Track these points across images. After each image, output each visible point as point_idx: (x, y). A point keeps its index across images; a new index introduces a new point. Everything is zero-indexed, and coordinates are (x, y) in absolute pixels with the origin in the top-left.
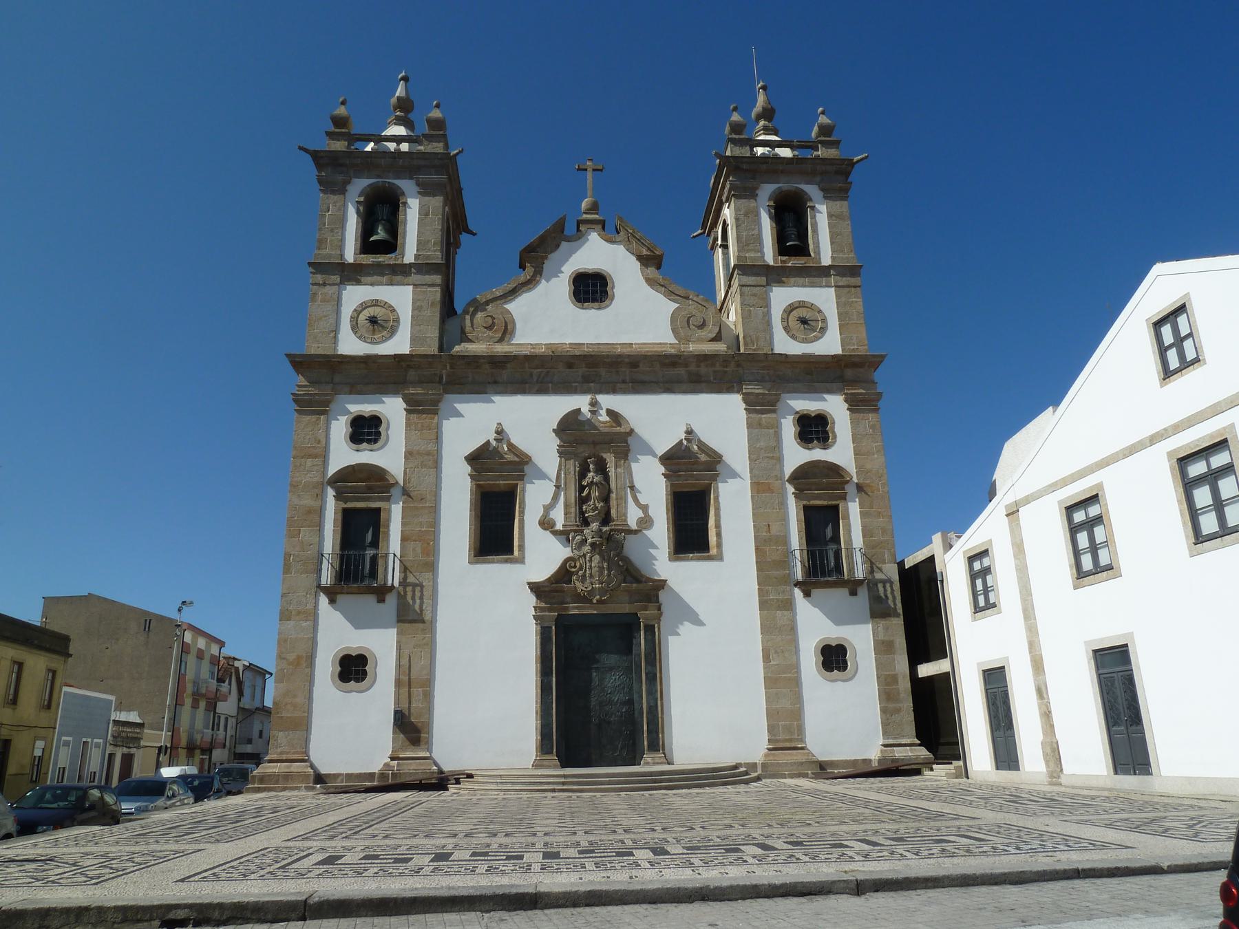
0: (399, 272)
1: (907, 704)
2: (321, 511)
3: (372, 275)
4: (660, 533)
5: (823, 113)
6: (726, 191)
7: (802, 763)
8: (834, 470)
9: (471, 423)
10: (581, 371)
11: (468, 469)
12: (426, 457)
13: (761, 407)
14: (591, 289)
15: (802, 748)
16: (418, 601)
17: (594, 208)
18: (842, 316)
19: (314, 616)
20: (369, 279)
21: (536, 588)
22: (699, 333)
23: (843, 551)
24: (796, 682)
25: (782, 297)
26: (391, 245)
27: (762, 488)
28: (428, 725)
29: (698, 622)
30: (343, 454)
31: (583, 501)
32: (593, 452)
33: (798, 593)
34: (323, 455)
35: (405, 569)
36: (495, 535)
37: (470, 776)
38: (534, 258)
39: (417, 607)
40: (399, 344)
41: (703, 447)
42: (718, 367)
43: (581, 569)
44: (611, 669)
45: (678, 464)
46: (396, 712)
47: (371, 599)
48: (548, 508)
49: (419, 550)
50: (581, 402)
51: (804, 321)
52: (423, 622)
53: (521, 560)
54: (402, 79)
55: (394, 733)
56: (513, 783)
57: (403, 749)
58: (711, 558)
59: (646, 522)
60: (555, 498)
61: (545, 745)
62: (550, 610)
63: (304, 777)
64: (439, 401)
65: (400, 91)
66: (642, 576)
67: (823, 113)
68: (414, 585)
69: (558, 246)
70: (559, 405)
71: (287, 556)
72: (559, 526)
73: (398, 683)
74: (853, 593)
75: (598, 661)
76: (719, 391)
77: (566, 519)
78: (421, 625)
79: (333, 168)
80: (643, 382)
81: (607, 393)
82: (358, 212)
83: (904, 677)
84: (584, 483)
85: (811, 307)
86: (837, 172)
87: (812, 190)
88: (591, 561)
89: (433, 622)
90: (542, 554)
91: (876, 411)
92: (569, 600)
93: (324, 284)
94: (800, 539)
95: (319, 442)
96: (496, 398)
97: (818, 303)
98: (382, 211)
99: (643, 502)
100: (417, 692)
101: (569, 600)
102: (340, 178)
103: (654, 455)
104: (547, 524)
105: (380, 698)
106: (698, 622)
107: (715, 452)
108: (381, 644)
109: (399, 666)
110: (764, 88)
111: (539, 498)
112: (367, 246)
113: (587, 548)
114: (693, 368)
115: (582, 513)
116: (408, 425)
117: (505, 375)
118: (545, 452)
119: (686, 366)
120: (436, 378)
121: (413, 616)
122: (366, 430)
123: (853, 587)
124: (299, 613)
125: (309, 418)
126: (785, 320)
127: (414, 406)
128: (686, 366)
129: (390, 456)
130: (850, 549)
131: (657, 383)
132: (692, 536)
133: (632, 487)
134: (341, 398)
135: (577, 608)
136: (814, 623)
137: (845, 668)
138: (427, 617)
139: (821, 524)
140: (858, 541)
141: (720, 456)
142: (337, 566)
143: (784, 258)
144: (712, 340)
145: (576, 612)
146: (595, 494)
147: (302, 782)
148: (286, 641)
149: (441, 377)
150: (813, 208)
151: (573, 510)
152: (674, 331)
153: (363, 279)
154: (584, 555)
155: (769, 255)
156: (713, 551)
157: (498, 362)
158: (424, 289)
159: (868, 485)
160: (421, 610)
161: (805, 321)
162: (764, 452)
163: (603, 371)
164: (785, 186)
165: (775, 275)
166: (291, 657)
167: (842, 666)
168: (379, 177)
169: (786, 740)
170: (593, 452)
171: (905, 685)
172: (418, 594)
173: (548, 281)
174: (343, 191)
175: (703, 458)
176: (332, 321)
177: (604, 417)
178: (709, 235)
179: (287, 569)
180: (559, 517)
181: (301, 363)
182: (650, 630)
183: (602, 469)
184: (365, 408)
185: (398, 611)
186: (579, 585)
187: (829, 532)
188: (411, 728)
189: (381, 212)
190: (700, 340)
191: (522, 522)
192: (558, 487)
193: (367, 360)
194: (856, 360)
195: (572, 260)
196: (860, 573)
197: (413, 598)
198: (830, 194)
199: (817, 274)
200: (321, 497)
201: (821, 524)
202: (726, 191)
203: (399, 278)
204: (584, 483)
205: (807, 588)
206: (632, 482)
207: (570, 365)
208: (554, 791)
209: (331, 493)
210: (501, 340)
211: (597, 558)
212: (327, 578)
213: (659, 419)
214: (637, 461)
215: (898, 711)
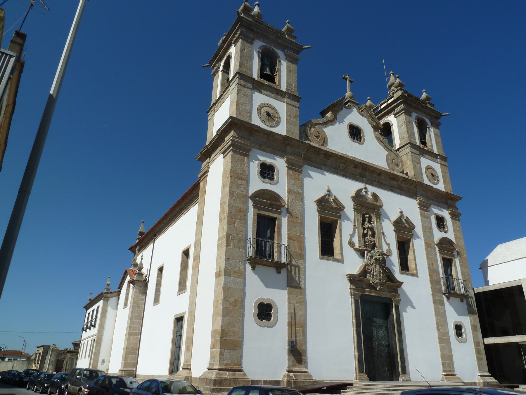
1: (484, 356)
2: (246, 211)
3: (267, 91)
5: (288, 23)
6: (237, 34)
8: (450, 242)
9: (319, 183)
10: (359, 171)
12: (297, 194)
13: (424, 207)
14: (355, 133)
16: (297, 276)
20: (266, 92)
24: (448, 341)
25: (259, 98)
27: (428, 245)
28: (305, 351)
29: (413, 307)
33: (249, 267)
35: (290, 256)
37: (351, 385)
39: (297, 279)
40: (281, 130)
41: (336, 200)
44: (380, 327)
45: (400, 226)
46: (289, 341)
48: (352, 236)
49: (297, 246)
52: (300, 288)
55: (289, 355)
56: (394, 390)
57: (294, 365)
59: (389, 251)
60: (354, 231)
61: (360, 369)
62: (358, 291)
64: (302, 167)
66: (395, 279)
67: (288, 23)
68: (296, 266)
70: (358, 185)
72: (357, 246)
73: (290, 324)
75: (374, 322)
76: (409, 197)
78: (300, 290)
81: (370, 185)
82: (259, 56)
85: (273, 108)
87: (280, 53)
89: (305, 289)
91: (459, 220)
92: (365, 286)
93: (245, 86)
95: (245, 172)
96: (326, 173)
97: (436, 169)
100: (299, 330)
102: (252, 36)
103: (390, 220)
104: (351, 244)
106: (413, 307)
107: (413, 224)
108: (280, 298)
109: (290, 313)
111: (347, 230)
113: (373, 261)
114: (399, 183)
116: (288, 175)
121: (294, 284)
124: (235, 272)
125: (238, 156)
126: (259, 110)
127: (291, 166)
129: (281, 187)
133: (383, 233)
134: (255, 151)
135: (368, 291)
137: (270, 319)
138: (302, 286)
140: (285, 241)
142: (255, 246)
145: (368, 294)
150: (280, 61)
153: (263, 91)
155: (256, 75)
158: (291, 107)
160: (300, 281)
161: (271, 116)
162: (428, 230)
163: (367, 174)
165: (258, 87)
166: (232, 300)
168: (267, 44)
171: (482, 347)
172: (297, 272)
173: (339, 124)
174: (252, 43)
176: (248, 107)
177: (370, 196)
178: (213, 67)
180: (356, 240)
182: (397, 308)
184: (268, 160)
187: (269, 233)
189: (269, 62)
192: (355, 226)
194: (453, 197)
195: (348, 117)
196: (284, 259)
197: (295, 273)
198: (291, 60)
199: (279, 94)
200: (245, 203)
202: (237, 34)
203: (279, 97)
205: (254, 263)
206: (383, 231)
209: (251, 203)
210: (323, 145)
211: (378, 266)
212: (250, 252)
213: (396, 205)
214: (384, 221)
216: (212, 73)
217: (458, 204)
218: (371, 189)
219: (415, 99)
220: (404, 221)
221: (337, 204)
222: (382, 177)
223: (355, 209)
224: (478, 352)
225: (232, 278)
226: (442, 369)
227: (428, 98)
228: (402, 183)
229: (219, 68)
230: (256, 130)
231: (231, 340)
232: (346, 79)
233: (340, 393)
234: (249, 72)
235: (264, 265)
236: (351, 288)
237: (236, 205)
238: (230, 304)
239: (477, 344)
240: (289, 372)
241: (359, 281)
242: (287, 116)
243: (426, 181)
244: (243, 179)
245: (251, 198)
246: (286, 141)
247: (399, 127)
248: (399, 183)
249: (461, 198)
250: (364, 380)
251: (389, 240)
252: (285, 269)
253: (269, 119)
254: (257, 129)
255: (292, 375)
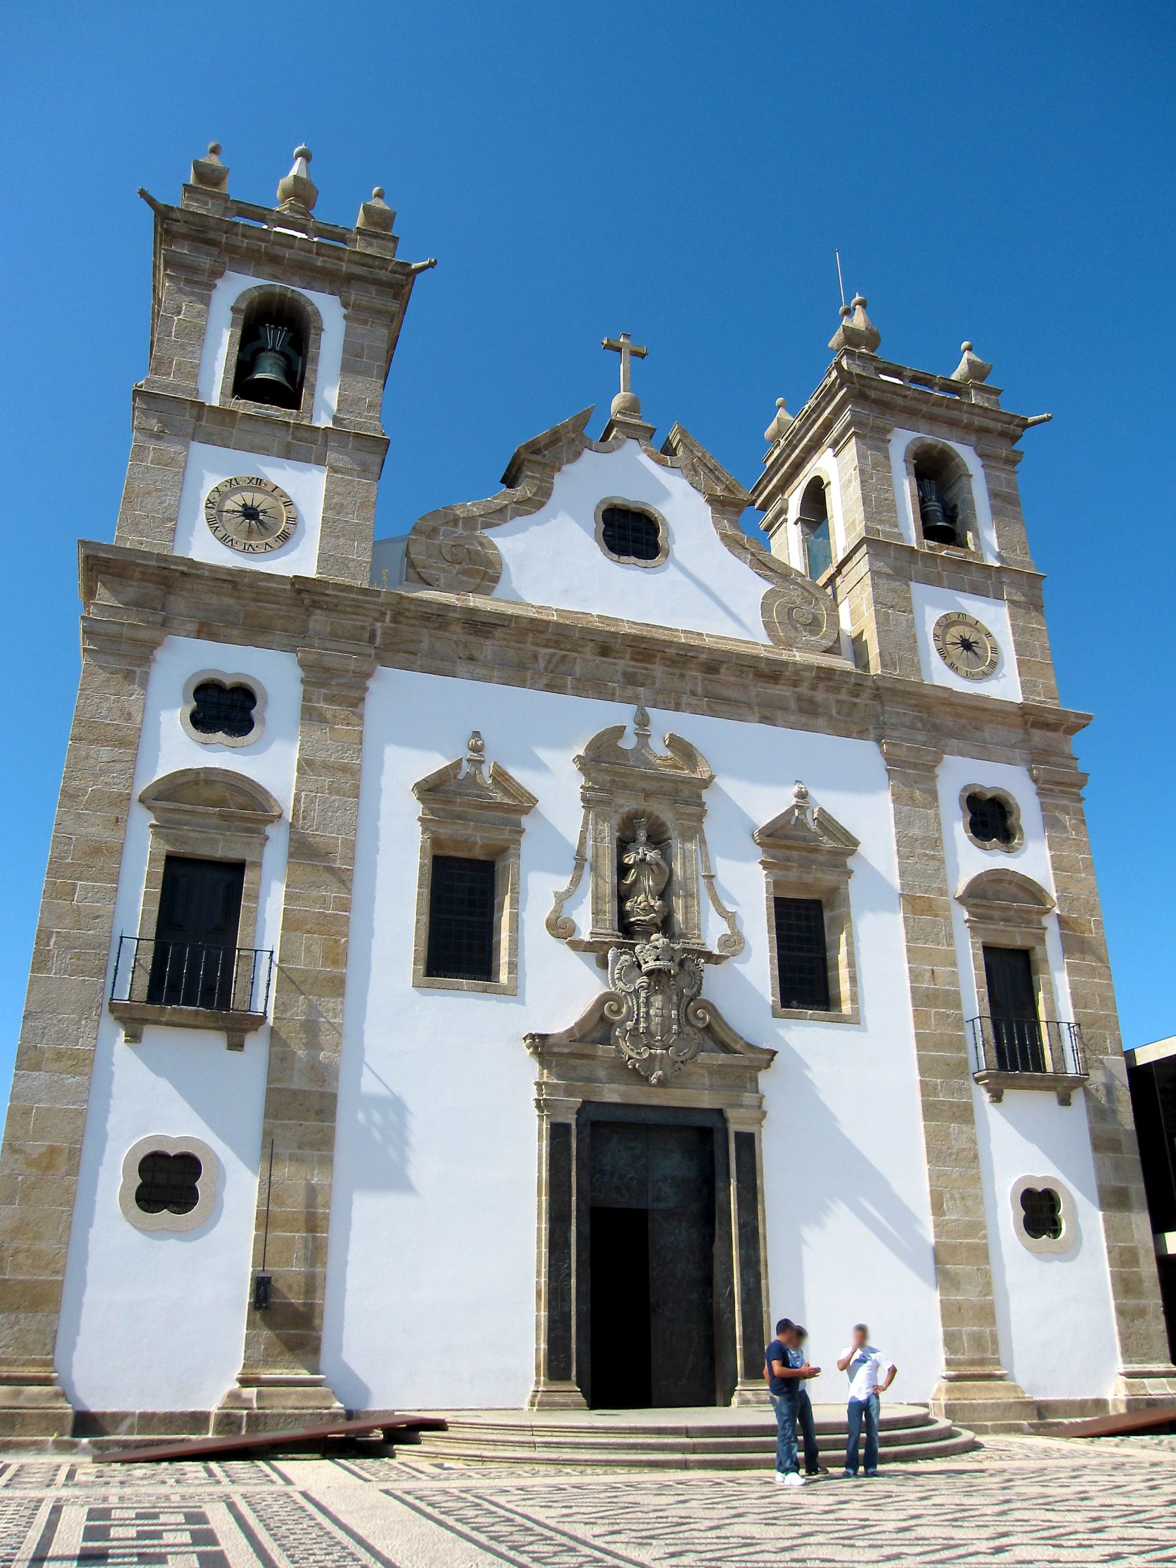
0: (304, 446)
1: (1154, 1300)
4: (758, 967)
5: (969, 349)
7: (1009, 1406)
8: (1030, 891)
9: (414, 730)
10: (623, 664)
11: (418, 808)
12: (338, 777)
13: (911, 776)
14: (631, 533)
15: (1001, 1378)
17: (632, 408)
18: (1020, 648)
19: (83, 1063)
21: (540, 1044)
22: (806, 637)
23: (1043, 1026)
24: (981, 1253)
25: (931, 607)
26: (289, 393)
27: (919, 906)
30: (177, 747)
31: (622, 896)
32: (645, 820)
33: (982, 1096)
34: (130, 741)
36: (462, 936)
37: (439, 1426)
38: (527, 472)
40: (301, 560)
42: (844, 696)
43: (629, 1017)
47: (216, 1041)
48: (561, 899)
49: (317, 950)
50: (620, 714)
51: (967, 645)
53: (512, 992)
54: (300, 154)
55: (251, 1324)
57: (267, 1363)
58: (841, 1020)
59: (734, 943)
61: (555, 1368)
63: (51, 1422)
65: (297, 168)
67: (969, 349)
69: (578, 455)
71: (43, 936)
74: (1065, 1101)
77: (596, 922)
79: (193, 238)
80: (727, 701)
83: (1147, 1251)
84: (629, 860)
85: (975, 625)
86: (1002, 434)
88: (648, 1004)
90: (555, 980)
92: (602, 1074)
94: (981, 1000)
97: (985, 621)
98: (274, 337)
99: (730, 908)
101: (602, 1074)
102: (206, 262)
104: (560, 928)
105: (223, 1246)
110: (863, 304)
111: (546, 898)
112: (244, 385)
114: (804, 689)
115: (622, 915)
117: (488, 648)
118: (557, 791)
119: (796, 684)
120: (358, 632)
122: (224, 708)
123: (1065, 1090)
124: (59, 1056)
128: (796, 684)
129: (270, 762)
130: (1054, 1023)
131: (749, 706)
132: (807, 979)
136: (1021, 1145)
139: (1012, 977)
140: (1067, 1013)
141: (856, 843)
143: (933, 544)
144: (828, 651)
146: (649, 882)
147: (47, 1431)
148: (26, 1112)
149: (372, 637)
151: (608, 907)
152: (766, 625)
154: (636, 992)
155: (912, 534)
156: (846, 1008)
157: (481, 625)
159: (1075, 920)
162: (920, 847)
163: (658, 670)
164: (929, 439)
167: (1053, 1227)
168: (274, 277)
169: (973, 1362)
170: (645, 820)
171: (1149, 1270)
175: (828, 843)
177: (658, 748)
178: (764, 507)
179: (40, 962)
181: (101, 566)
183: (658, 839)
185: (271, 1069)
186: (626, 1047)
188: (286, 1315)
190: (808, 648)
191: (515, 919)
193: (232, 580)
201: (1012, 977)
204: (629, 860)
207: (605, 651)
208: (685, 1465)
211: (658, 1001)
212: (131, 982)
213: (754, 778)
215: (1141, 1312)
216: (762, 527)
217: (1076, 744)
218: (666, 722)
219: (915, 380)
220: (813, 826)
221: (506, 792)
222: (725, 674)
223: (588, 803)
224: (1125, 1285)
225: (43, 1074)
226: (942, 1355)
227: (976, 371)
228: (813, 688)
229: (783, 511)
230: (183, 573)
231: (22, 1281)
232: (619, 350)
233: (392, 1456)
234: (185, 383)
235: (167, 1024)
236: (539, 1085)
237: (83, 831)
238: (30, 1163)
239: (1123, 1258)
240: (245, 1382)
241: (572, 1055)
242: (325, 510)
243: (940, 674)
244: (122, 743)
245: (960, 900)
246: (304, 595)
247: (845, 486)
248: (804, 689)
249: (1089, 718)
250: (564, 1407)
251: (737, 900)
252: (1081, 1089)
253: (250, 531)
254: (184, 569)
255: (251, 1392)
